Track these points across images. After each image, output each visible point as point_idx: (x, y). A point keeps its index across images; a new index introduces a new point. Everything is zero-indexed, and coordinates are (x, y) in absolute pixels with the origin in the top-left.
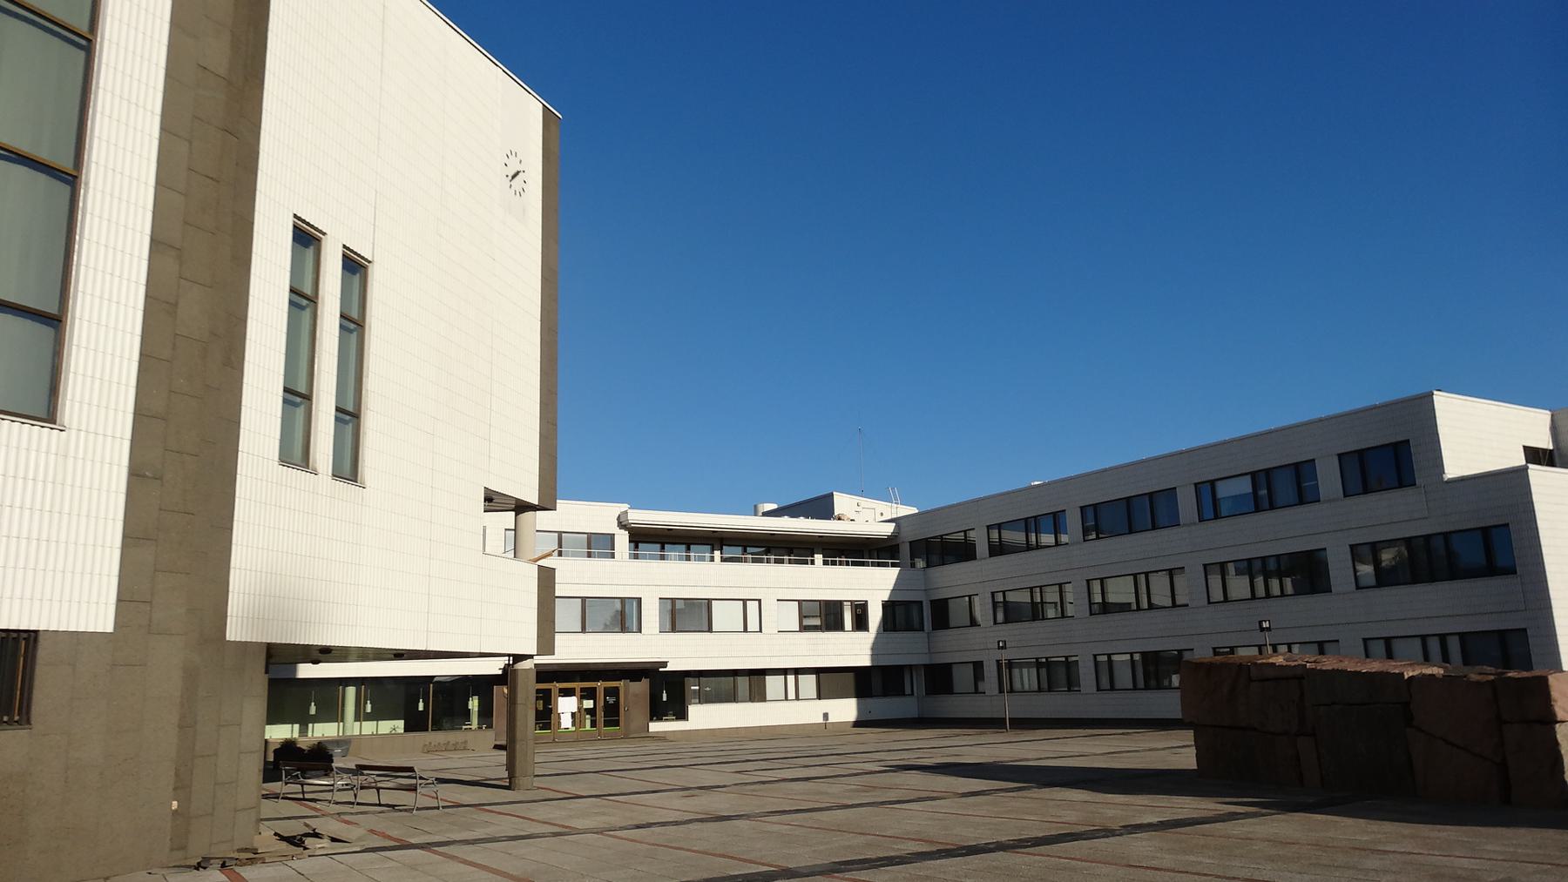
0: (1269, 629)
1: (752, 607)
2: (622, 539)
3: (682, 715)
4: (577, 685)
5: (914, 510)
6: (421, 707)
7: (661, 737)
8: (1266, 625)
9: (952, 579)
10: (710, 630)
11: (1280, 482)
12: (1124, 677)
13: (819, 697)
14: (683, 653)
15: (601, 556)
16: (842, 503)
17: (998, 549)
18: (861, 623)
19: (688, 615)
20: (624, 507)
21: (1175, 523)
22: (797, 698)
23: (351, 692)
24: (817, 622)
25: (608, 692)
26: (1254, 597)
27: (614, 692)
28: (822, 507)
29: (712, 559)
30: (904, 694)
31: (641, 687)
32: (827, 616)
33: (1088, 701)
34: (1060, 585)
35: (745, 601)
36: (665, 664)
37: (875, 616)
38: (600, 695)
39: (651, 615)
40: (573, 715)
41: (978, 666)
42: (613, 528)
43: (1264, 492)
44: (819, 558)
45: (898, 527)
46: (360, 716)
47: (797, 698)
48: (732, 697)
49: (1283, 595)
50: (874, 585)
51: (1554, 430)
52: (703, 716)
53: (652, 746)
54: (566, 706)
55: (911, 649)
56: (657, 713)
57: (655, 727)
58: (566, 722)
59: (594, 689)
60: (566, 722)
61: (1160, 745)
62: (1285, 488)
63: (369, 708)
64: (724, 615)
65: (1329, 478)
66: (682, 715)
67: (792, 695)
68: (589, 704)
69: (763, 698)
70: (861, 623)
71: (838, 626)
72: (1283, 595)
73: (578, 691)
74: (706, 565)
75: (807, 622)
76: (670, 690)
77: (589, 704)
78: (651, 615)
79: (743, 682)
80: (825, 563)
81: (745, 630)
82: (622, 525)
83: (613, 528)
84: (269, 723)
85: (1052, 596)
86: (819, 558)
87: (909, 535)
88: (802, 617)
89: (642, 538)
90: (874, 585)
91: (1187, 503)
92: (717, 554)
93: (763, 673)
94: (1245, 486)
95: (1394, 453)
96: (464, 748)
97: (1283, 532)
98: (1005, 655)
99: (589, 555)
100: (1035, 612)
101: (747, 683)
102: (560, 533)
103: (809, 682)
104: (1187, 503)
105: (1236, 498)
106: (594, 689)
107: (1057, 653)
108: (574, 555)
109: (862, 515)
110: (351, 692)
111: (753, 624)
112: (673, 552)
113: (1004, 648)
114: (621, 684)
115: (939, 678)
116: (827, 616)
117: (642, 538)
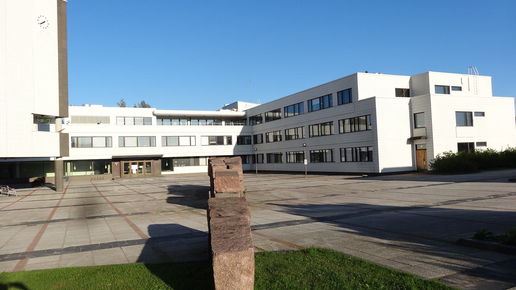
0: (305, 146)
1: (193, 139)
2: (154, 118)
3: (172, 170)
4: (137, 162)
5: (254, 105)
6: (106, 167)
7: (163, 176)
8: (305, 145)
9: (259, 129)
11: (325, 102)
14: (168, 152)
15: (148, 124)
17: (268, 119)
18: (230, 142)
19: (167, 141)
23: (69, 164)
24: (215, 142)
25: (147, 163)
26: (351, 132)
27: (150, 163)
28: (234, 106)
29: (180, 124)
30: (323, 162)
31: (160, 161)
32: (219, 140)
35: (190, 137)
36: (162, 155)
37: (234, 141)
42: (151, 115)
43: (322, 104)
44: (223, 123)
45: (246, 112)
46: (72, 170)
48: (188, 164)
49: (355, 131)
50: (235, 131)
51: (411, 82)
52: (178, 170)
54: (134, 168)
55: (246, 150)
57: (163, 173)
58: (134, 172)
59: (150, 163)
63: (75, 168)
64: (184, 141)
66: (172, 170)
69: (198, 165)
70: (230, 142)
72: (355, 131)
74: (186, 126)
76: (167, 163)
77: (141, 167)
79: (192, 160)
80: (225, 125)
81: (179, 145)
82: (154, 115)
83: (151, 115)
86: (223, 123)
87: (250, 115)
88: (209, 141)
89: (161, 118)
90: (235, 131)
92: (189, 122)
93: (198, 157)
95: (347, 94)
96: (103, 179)
106: (150, 163)
108: (140, 124)
109: (241, 110)
110: (69, 164)
111: (193, 143)
112: (175, 122)
114: (151, 161)
115: (255, 158)
116: (219, 140)
117: (161, 118)
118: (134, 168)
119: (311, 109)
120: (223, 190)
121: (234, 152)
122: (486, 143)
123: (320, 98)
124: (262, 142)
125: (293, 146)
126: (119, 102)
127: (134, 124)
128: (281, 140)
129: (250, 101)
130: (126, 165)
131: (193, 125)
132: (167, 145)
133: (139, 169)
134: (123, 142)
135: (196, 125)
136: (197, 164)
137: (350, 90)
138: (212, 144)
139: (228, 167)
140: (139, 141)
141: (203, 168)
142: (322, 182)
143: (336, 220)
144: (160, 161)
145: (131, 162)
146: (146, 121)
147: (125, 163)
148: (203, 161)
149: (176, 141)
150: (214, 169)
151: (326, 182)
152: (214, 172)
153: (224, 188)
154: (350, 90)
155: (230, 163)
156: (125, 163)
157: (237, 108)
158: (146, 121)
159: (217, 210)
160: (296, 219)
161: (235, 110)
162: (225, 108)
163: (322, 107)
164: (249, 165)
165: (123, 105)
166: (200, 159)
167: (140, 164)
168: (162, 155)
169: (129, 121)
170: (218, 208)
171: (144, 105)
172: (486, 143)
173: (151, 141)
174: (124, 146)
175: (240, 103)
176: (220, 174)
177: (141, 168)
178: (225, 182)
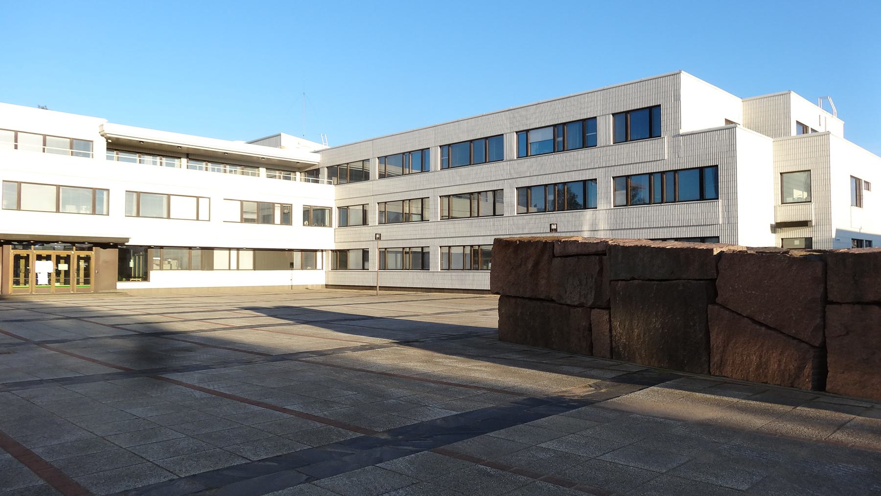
2: (100, 145)
3: (145, 277)
7: (123, 293)
8: (554, 227)
10: (19, 208)
12: (457, 263)
13: (255, 269)
14: (138, 233)
16: (285, 138)
19: (140, 203)
20: (103, 121)
21: (500, 159)
22: (238, 269)
24: (255, 217)
28: (274, 140)
31: (112, 255)
34: (422, 199)
36: (127, 240)
38: (74, 261)
40: (49, 274)
41: (365, 253)
47: (238, 269)
54: (43, 269)
56: (125, 274)
57: (122, 285)
58: (43, 280)
60: (43, 280)
61: (474, 308)
62: (573, 135)
64: (181, 207)
65: (606, 130)
66: (145, 277)
67: (234, 265)
68: (63, 267)
73: (54, 258)
75: (246, 216)
77: (63, 267)
78: (118, 202)
84: (120, 280)
85: (416, 208)
89: (116, 146)
91: (511, 145)
93: (212, 249)
94: (549, 135)
98: (383, 244)
100: (403, 218)
101: (203, 257)
102: (45, 136)
103: (247, 258)
104: (511, 145)
105: (542, 143)
107: (416, 244)
108: (58, 152)
112: (148, 159)
113: (379, 238)
117: (116, 146)
118: (43, 269)
119: (525, 152)
121: (622, 189)
122: (718, 237)
123: (555, 126)
127: (16, 147)
131: (51, 151)
132: (138, 215)
134: (16, 197)
135: (64, 153)
138: (247, 221)
140: (62, 197)
146: (80, 147)
158: (80, 147)
164: (323, 273)
166: (215, 252)
168: (127, 240)
172: (718, 237)
173: (96, 200)
174: (19, 208)
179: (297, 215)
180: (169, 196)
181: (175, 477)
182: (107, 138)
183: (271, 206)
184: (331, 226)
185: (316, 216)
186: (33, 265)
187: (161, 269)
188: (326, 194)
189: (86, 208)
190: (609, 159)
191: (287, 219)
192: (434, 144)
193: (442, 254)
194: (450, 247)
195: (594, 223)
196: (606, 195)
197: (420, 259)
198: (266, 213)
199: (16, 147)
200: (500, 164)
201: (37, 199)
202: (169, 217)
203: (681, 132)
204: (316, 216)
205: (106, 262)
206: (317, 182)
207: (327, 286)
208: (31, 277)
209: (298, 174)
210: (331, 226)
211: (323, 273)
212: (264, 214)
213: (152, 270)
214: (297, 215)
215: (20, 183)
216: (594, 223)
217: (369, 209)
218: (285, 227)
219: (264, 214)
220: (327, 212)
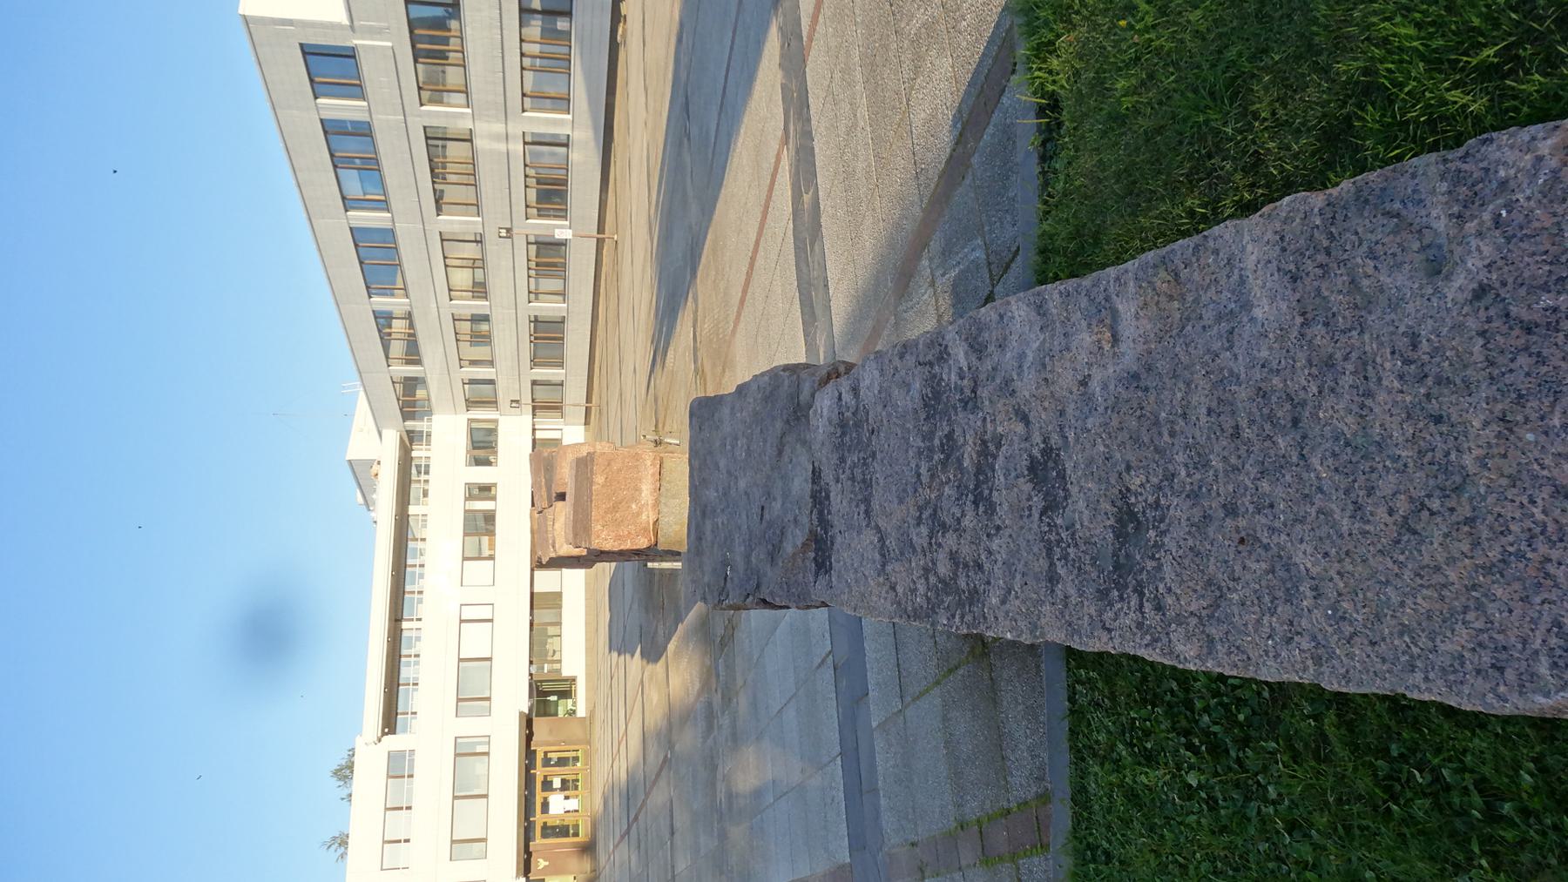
0: (509, 230)
1: (468, 613)
2: (393, 742)
3: (573, 680)
8: (504, 233)
11: (351, 147)
14: (513, 698)
15: (412, 762)
19: (470, 700)
25: (547, 762)
28: (362, 473)
33: (576, 311)
36: (521, 714)
39: (471, 726)
40: (567, 798)
53: (599, 715)
54: (559, 805)
58: (573, 804)
60: (573, 804)
64: (476, 642)
66: (573, 680)
69: (559, 595)
71: (490, 518)
73: (545, 794)
76: (546, 695)
77: (557, 783)
78: (471, 726)
81: (491, 621)
89: (390, 723)
93: (532, 594)
97: (403, 165)
99: (411, 776)
102: (387, 809)
108: (410, 791)
109: (374, 443)
111: (485, 613)
112: (406, 673)
113: (509, 230)
118: (559, 805)
120: (648, 516)
124: (491, 382)
125: (509, 268)
126: (333, 854)
127: (407, 841)
128: (486, 318)
129: (349, 415)
130: (548, 831)
131: (411, 766)
132: (489, 699)
133: (565, 785)
136: (554, 600)
137: (308, 52)
139: (562, 497)
141: (573, 585)
142: (634, 175)
143: (805, 34)
144: (537, 722)
145: (539, 819)
146: (399, 768)
147: (544, 836)
148: (548, 581)
149: (472, 668)
150: (566, 549)
151: (635, 162)
152: (576, 552)
153: (639, 514)
154: (308, 52)
155: (549, 489)
156: (544, 836)
157: (369, 464)
158: (399, 768)
159: (772, 557)
160: (789, 209)
161: (375, 467)
162: (368, 504)
163: (370, 166)
165: (342, 841)
167: (547, 785)
168: (521, 714)
169: (398, 825)
170: (759, 556)
171: (345, 773)
175: (352, 454)
176: (581, 525)
177: (564, 782)
178: (615, 509)
179: (482, 475)
180: (460, 660)
181: (830, 660)
182: (384, 734)
183: (470, 516)
184: (496, 421)
185: (482, 447)
186: (555, 817)
187: (560, 661)
188: (447, 431)
189: (479, 765)
190: (390, 102)
191: (486, 491)
192: (364, 307)
193: (533, 109)
194: (524, 95)
195: (495, 137)
196: (450, 114)
197: (547, 337)
198: (481, 523)
199: (407, 841)
200: (399, 233)
201: (471, 820)
202: (490, 659)
203: (346, 22)
204: (482, 447)
205: (551, 731)
206: (429, 435)
207: (587, 423)
208: (569, 820)
209: (414, 454)
210: (496, 421)
211: (567, 429)
212: (481, 526)
213: (559, 671)
214: (482, 475)
215: (453, 842)
216: (495, 137)
217: (467, 378)
218: (500, 492)
219: (481, 526)
220: (474, 425)
